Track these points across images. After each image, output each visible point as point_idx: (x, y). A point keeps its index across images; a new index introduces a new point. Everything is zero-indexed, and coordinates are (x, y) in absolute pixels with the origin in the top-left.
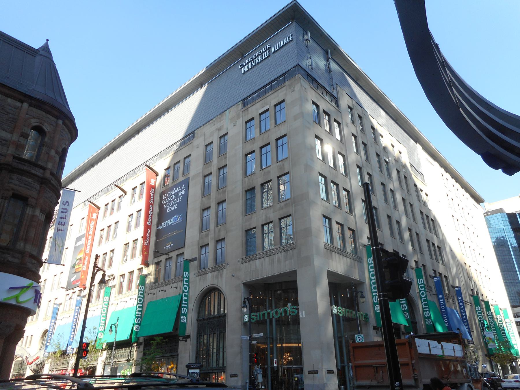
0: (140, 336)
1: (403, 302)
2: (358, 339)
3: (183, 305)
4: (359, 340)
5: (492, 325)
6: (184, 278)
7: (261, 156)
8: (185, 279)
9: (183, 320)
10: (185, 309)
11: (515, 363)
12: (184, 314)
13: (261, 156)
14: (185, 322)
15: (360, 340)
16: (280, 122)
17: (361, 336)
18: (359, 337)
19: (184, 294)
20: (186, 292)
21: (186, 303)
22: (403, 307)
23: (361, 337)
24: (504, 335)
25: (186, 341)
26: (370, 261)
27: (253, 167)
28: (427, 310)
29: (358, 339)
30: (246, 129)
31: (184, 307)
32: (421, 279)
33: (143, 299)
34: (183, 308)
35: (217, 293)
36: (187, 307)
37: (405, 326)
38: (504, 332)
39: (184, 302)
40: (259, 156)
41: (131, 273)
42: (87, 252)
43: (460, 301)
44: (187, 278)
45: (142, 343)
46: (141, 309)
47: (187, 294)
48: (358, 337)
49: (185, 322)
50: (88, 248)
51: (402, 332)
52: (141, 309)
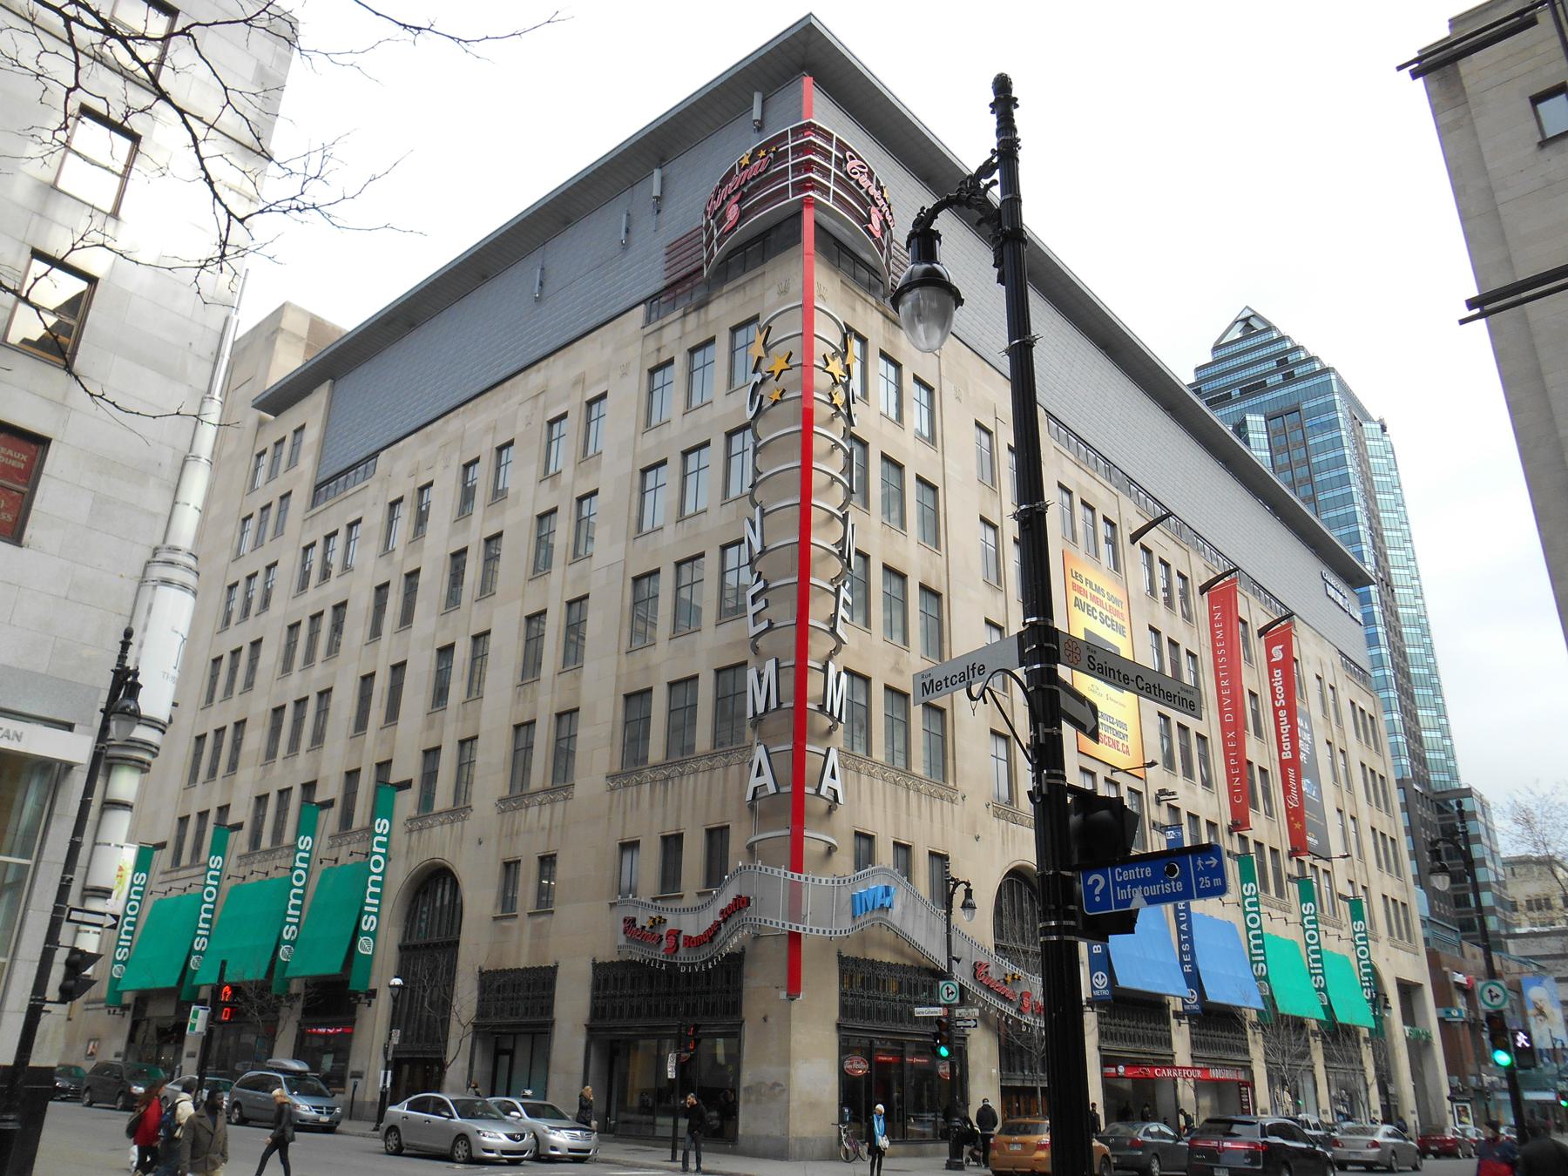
0: (293, 975)
1: (1317, 971)
2: (945, 992)
4: (1492, 998)
6: (209, 869)
7: (728, 458)
8: (377, 839)
9: (365, 946)
10: (373, 918)
11: (1434, 1145)
12: (368, 933)
13: (728, 458)
14: (370, 953)
16: (742, 383)
17: (1499, 985)
18: (948, 988)
19: (128, 919)
21: (376, 902)
22: (1316, 981)
23: (952, 988)
24: (1261, 955)
25: (369, 1005)
26: (119, 955)
27: (662, 504)
28: (1262, 961)
29: (945, 992)
30: (651, 393)
31: (291, 924)
32: (1310, 904)
33: (217, 890)
34: (366, 917)
35: (448, 881)
36: (1323, 975)
37: (1258, 1011)
38: (1261, 942)
39: (368, 900)
40: (677, 479)
41: (284, 794)
42: (1287, 755)
43: (1183, 937)
44: (384, 836)
45: (206, 1000)
46: (210, 916)
47: (380, 878)
49: (370, 953)
50: (1287, 745)
51: (1312, 1031)
52: (210, 916)
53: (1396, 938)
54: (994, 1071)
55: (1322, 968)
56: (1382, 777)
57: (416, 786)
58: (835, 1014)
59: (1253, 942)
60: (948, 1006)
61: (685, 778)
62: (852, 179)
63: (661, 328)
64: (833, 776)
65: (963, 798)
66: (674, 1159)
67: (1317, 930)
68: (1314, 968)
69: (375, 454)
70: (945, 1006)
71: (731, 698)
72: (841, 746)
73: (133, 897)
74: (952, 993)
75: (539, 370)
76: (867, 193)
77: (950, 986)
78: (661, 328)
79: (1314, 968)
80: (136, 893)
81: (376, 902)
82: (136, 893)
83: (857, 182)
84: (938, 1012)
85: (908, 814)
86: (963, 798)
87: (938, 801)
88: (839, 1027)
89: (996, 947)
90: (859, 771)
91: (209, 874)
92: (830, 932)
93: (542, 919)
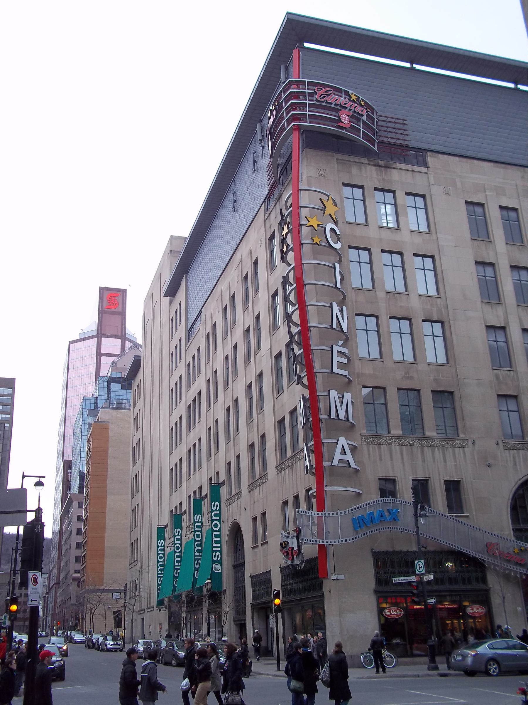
2: (418, 566)
3: (214, 549)
5: (198, 541)
14: (220, 571)
15: (421, 569)
18: (419, 565)
20: (198, 541)
21: (219, 545)
23: (421, 565)
44: (217, 511)
47: (219, 533)
48: (418, 564)
54: (519, 609)
55: (220, 547)
57: (227, 482)
58: (372, 585)
59: (160, 568)
60: (421, 575)
61: (297, 463)
62: (323, 102)
63: (269, 215)
64: (344, 452)
65: (474, 443)
66: (279, 669)
67: (219, 521)
68: (197, 556)
69: (200, 312)
70: (418, 575)
71: (372, 402)
72: (364, 432)
73: (160, 552)
74: (421, 567)
75: (239, 250)
76: (336, 105)
77: (420, 563)
78: (269, 215)
79: (197, 556)
80: (161, 550)
81: (219, 545)
82: (161, 550)
83: (327, 102)
84: (412, 579)
85: (424, 461)
86: (474, 443)
87: (450, 450)
88: (376, 592)
89: (515, 530)
90: (379, 444)
91: (196, 534)
92: (339, 542)
93: (265, 546)
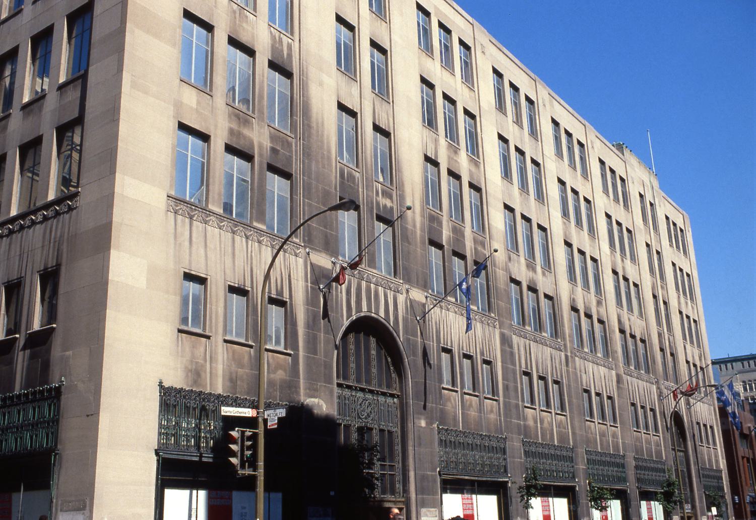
53: (632, 368)
56: (688, 275)
